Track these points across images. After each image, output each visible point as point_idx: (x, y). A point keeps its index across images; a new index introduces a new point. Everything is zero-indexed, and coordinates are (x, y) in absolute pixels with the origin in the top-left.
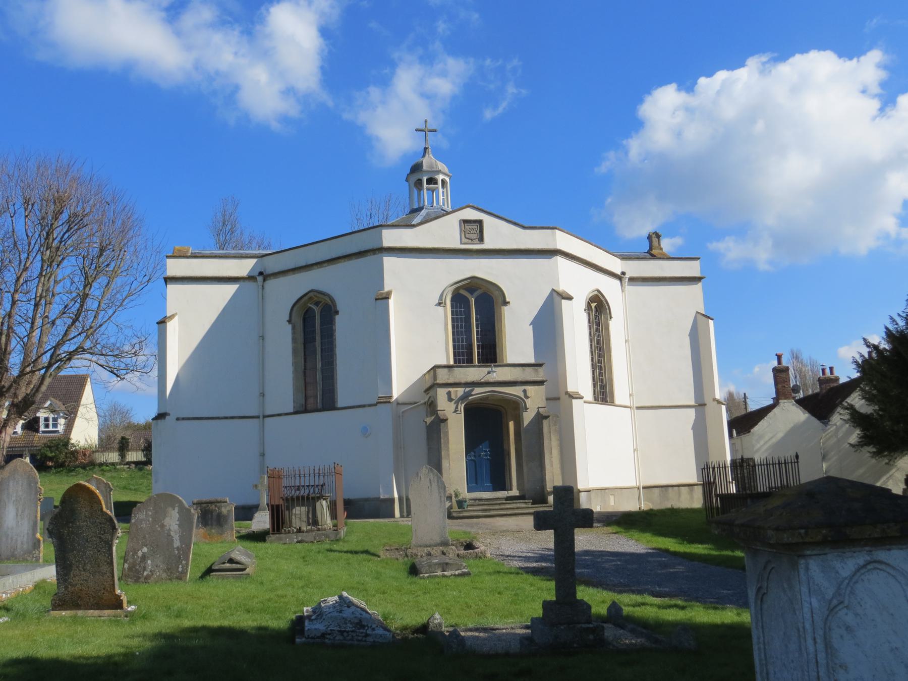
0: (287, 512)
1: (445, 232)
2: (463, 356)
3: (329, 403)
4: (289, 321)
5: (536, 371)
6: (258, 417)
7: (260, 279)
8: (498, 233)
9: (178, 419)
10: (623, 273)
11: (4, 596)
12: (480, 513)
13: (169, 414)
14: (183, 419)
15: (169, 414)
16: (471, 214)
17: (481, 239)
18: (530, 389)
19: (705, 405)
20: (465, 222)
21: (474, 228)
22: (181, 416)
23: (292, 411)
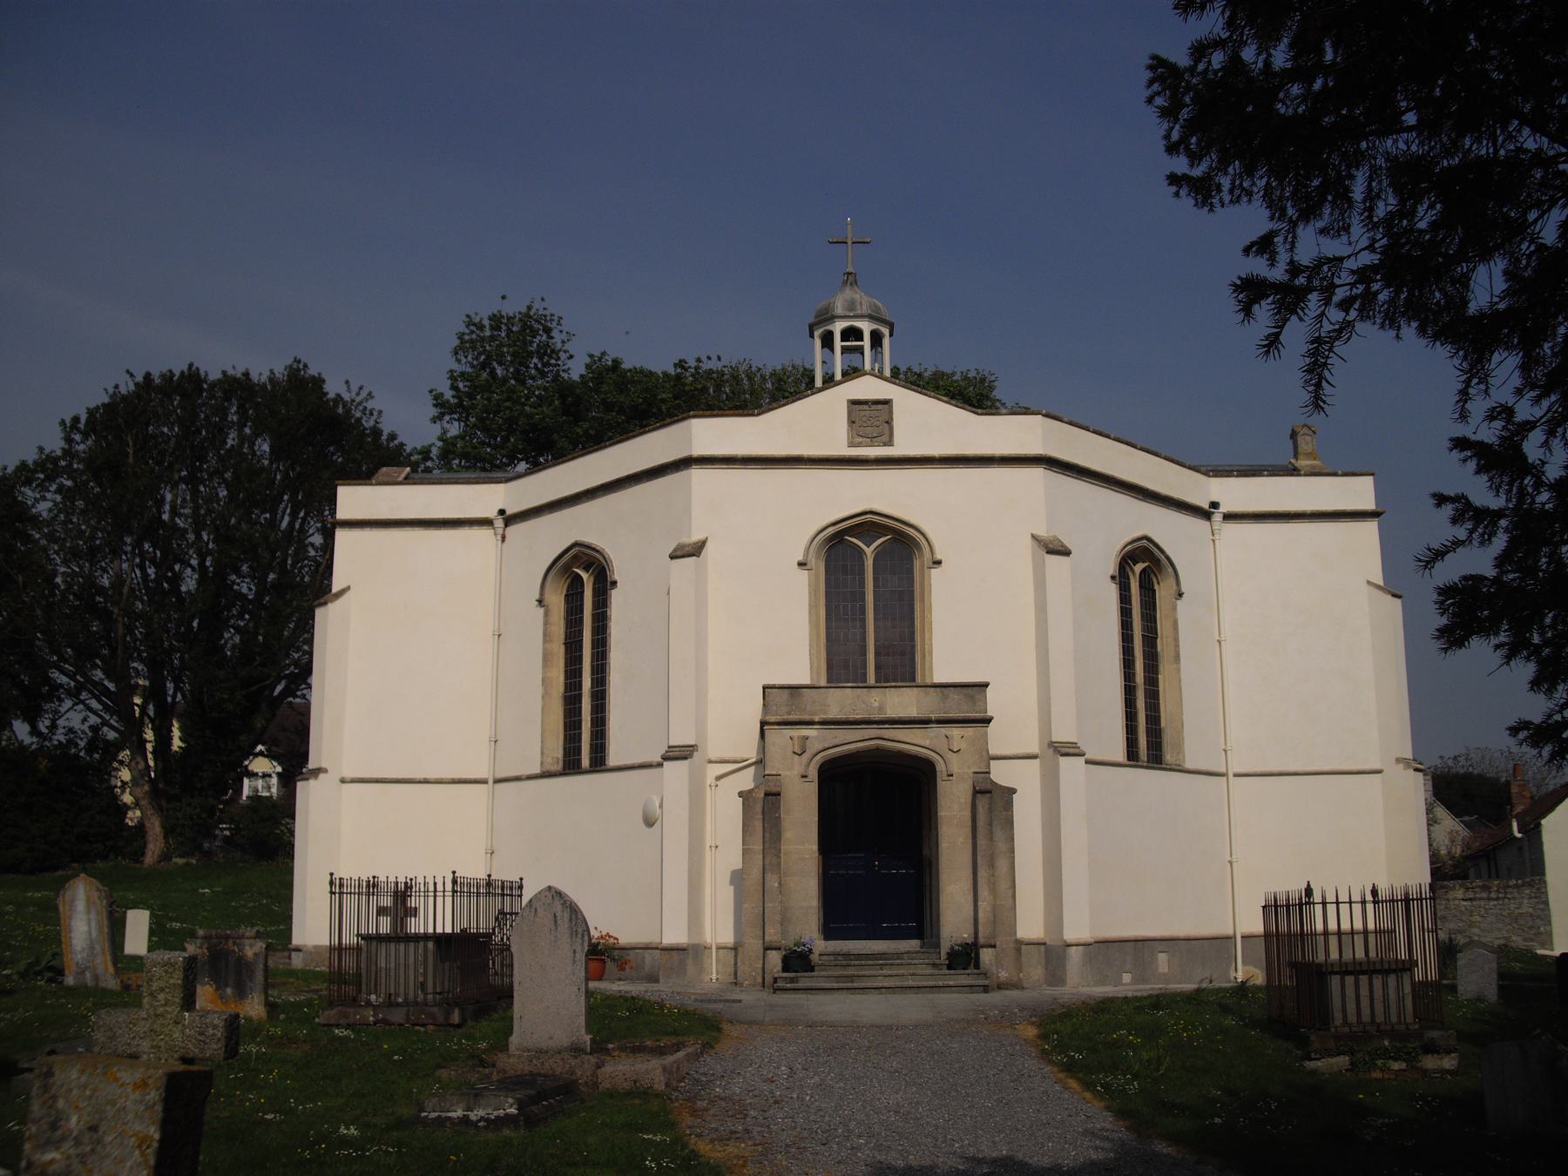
0: (94, 934)
1: (815, 422)
2: (841, 666)
3: (599, 763)
4: (540, 602)
5: (972, 697)
6: (484, 782)
7: (499, 523)
8: (924, 422)
9: (343, 781)
10: (1215, 505)
11: (1217, 1120)
12: (835, 985)
13: (326, 771)
14: (353, 781)
15: (326, 771)
16: (868, 388)
17: (889, 443)
18: (956, 732)
19: (988, 721)
20: (854, 403)
21: (871, 419)
22: (349, 775)
23: (538, 771)
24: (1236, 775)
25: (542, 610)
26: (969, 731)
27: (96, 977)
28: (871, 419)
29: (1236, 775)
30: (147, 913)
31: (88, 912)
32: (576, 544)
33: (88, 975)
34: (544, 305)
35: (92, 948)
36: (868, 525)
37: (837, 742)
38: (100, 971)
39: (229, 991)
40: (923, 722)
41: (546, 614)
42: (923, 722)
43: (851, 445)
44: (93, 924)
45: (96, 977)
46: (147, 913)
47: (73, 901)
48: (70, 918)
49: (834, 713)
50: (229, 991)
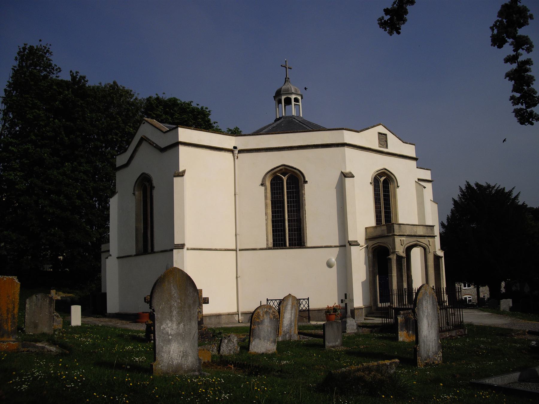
0: (292, 319)
7: (236, 152)
24: (240, 250)
25: (263, 188)
26: (430, 239)
27: (291, 336)
28: (383, 138)
29: (240, 250)
30: (80, 307)
31: (292, 310)
32: (385, 169)
33: (287, 335)
34: (50, 47)
35: (291, 324)
36: (286, 170)
37: (409, 241)
38: (292, 333)
39: (411, 332)
40: (424, 236)
41: (266, 189)
42: (424, 236)
43: (379, 147)
44: (293, 314)
45: (291, 336)
46: (80, 307)
47: (287, 305)
48: (284, 313)
49: (408, 233)
50: (411, 332)
